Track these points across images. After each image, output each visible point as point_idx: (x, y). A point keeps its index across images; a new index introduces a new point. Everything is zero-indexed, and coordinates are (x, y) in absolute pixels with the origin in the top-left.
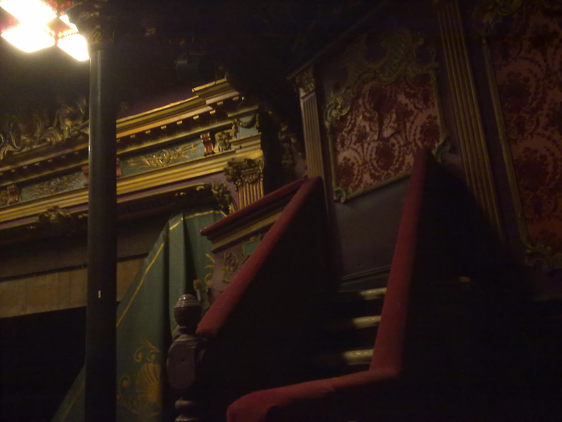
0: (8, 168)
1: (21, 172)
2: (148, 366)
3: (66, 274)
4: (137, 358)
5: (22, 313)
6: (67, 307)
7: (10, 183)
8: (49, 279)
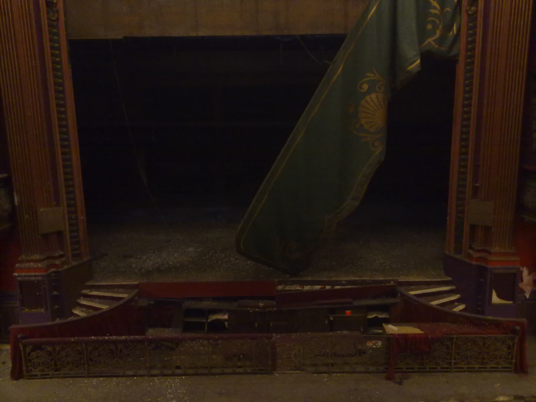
2: (371, 98)
4: (361, 88)
5: (194, 34)
6: (254, 34)
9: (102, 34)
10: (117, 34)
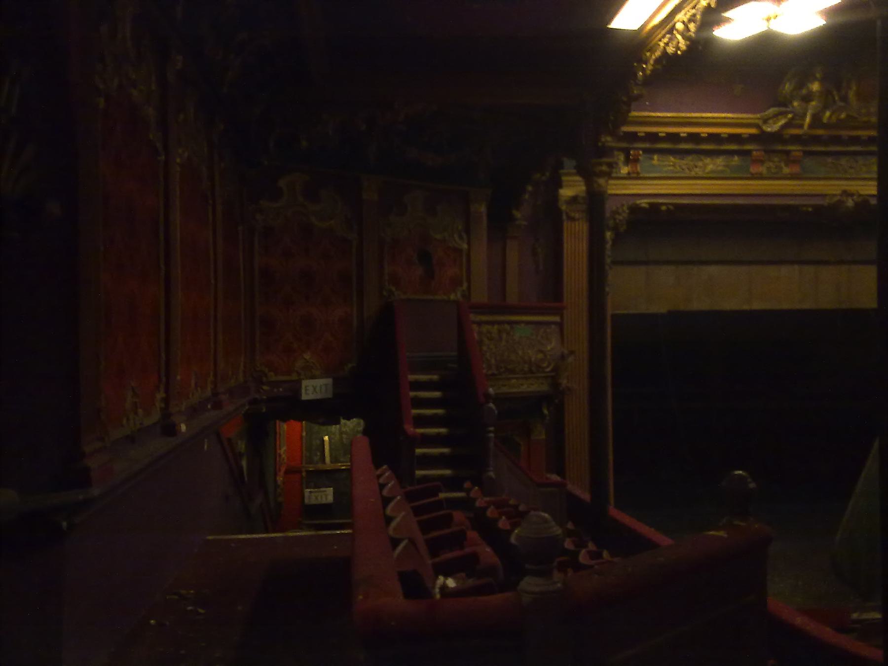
0: (820, 132)
1: (837, 140)
3: (810, 270)
7: (800, 148)
8: (784, 271)
9: (643, 308)
10: (660, 308)
